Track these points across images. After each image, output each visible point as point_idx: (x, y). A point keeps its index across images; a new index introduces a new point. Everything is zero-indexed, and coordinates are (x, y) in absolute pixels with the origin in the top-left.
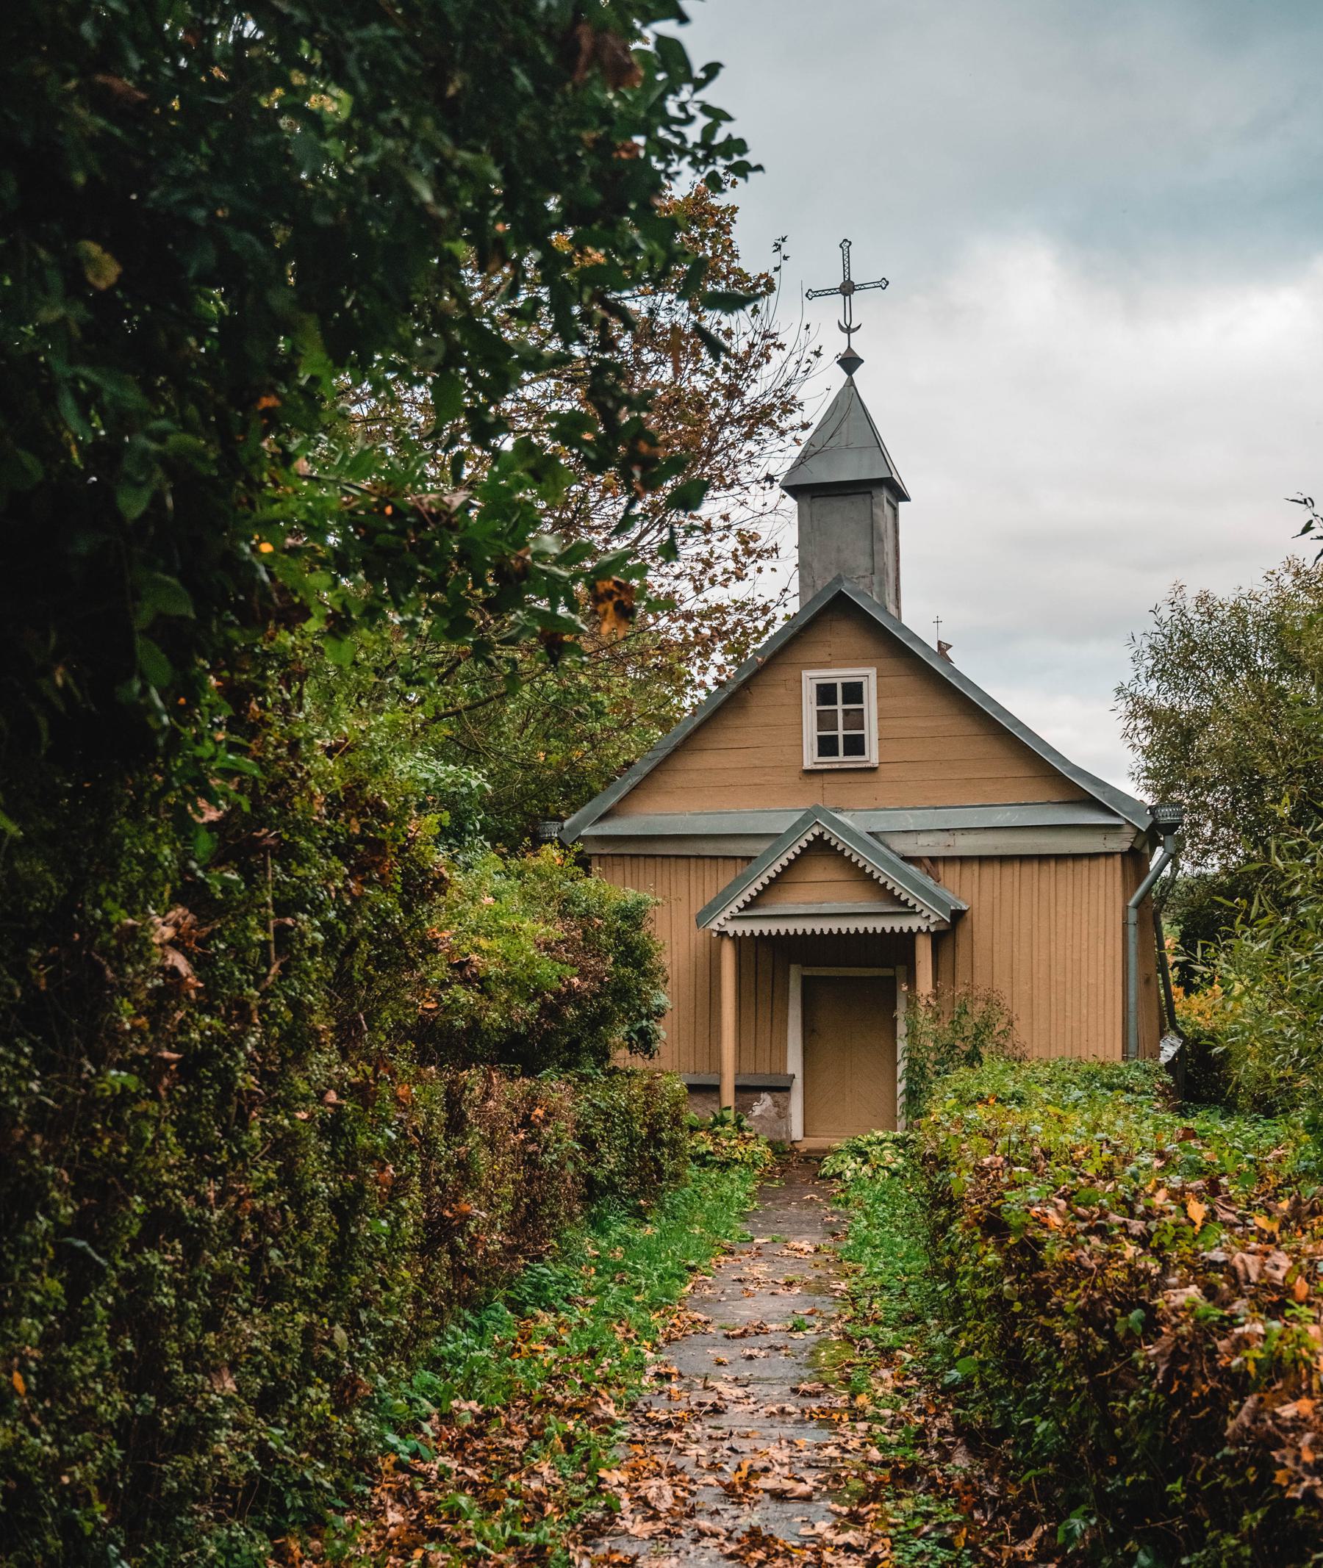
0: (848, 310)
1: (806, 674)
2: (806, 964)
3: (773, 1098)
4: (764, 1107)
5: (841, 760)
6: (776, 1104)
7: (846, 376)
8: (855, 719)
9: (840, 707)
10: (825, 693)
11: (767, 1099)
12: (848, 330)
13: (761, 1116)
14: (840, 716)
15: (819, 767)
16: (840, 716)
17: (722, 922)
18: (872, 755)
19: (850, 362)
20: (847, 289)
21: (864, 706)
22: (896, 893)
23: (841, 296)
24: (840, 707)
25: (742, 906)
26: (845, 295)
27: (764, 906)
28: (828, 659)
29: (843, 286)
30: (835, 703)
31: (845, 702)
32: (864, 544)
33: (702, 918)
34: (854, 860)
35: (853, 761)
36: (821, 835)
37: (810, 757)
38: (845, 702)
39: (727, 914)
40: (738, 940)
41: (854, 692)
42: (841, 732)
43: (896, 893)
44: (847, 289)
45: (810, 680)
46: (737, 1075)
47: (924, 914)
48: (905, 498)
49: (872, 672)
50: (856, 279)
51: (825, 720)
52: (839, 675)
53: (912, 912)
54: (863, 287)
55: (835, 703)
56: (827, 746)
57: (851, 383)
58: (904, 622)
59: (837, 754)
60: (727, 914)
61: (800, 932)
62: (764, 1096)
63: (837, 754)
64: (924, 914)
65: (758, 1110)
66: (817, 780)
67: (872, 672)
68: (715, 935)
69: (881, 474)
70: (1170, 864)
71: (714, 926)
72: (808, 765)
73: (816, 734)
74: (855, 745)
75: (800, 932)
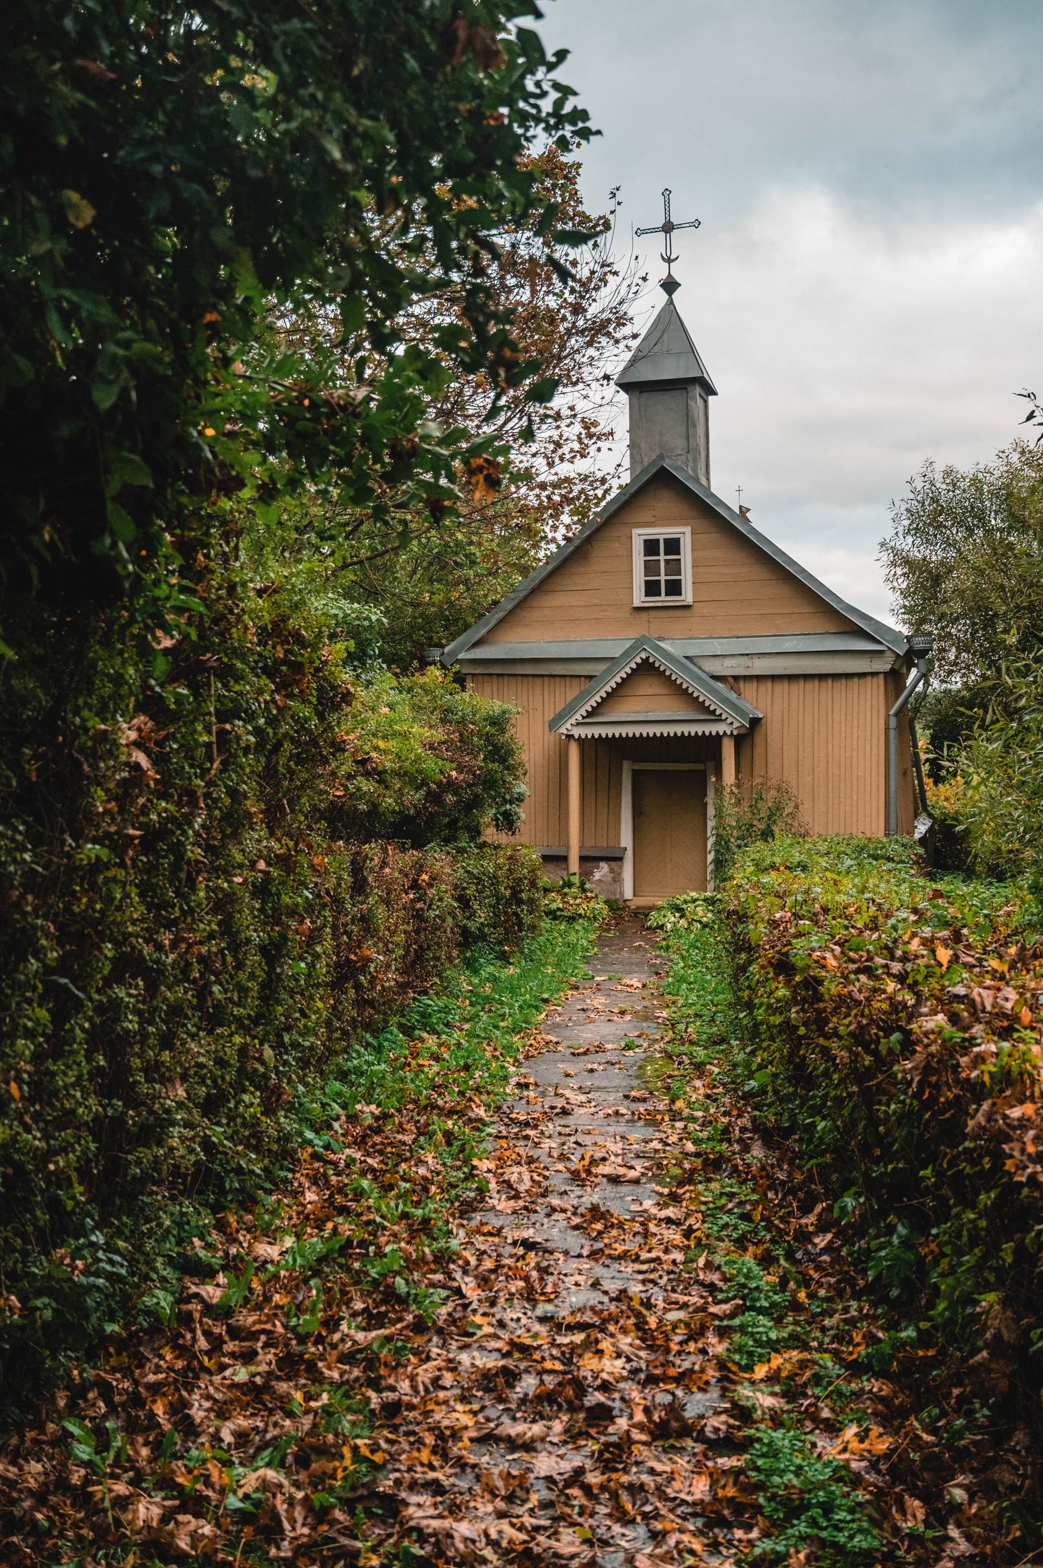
0: (668, 244)
1: (636, 532)
2: (635, 760)
5: (663, 599)
6: (612, 871)
7: (667, 297)
8: (674, 567)
9: (662, 557)
10: (651, 547)
12: (669, 261)
14: (662, 564)
16: (662, 564)
18: (688, 596)
19: (670, 286)
20: (668, 228)
21: (681, 557)
23: (663, 234)
27: (602, 714)
29: (664, 225)
31: (666, 554)
33: (554, 724)
36: (648, 658)
37: (639, 598)
38: (666, 554)
39: (573, 721)
40: (582, 742)
41: (673, 546)
42: (663, 578)
44: (668, 228)
45: (639, 536)
46: (581, 848)
48: (714, 393)
49: (688, 530)
50: (675, 220)
51: (650, 568)
52: (661, 533)
53: (719, 720)
54: (680, 226)
56: (652, 588)
57: (671, 302)
60: (573, 721)
62: (602, 864)
65: (597, 875)
67: (688, 530)
71: (563, 730)
72: (637, 603)
73: (644, 579)
74: (674, 588)
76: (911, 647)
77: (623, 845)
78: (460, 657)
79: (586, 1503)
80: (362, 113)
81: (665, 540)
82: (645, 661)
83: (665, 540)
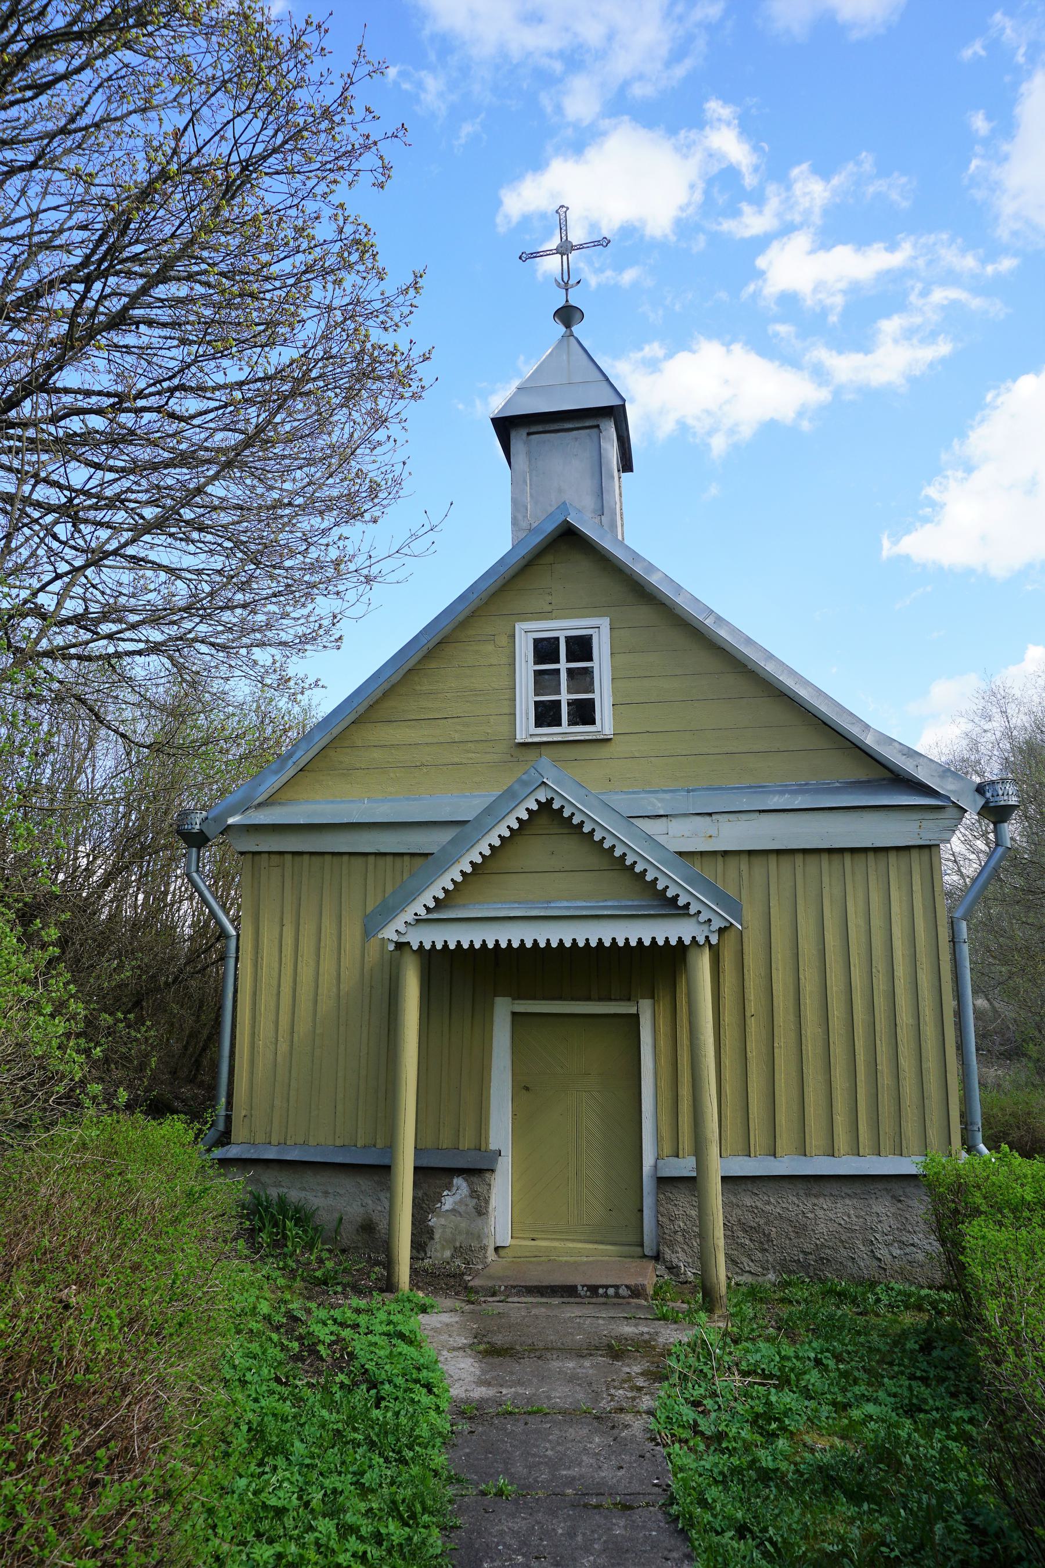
1: (520, 627)
2: (518, 996)
3: (470, 1185)
4: (457, 1197)
5: (565, 730)
6: (474, 1194)
8: (582, 678)
9: (563, 665)
10: (545, 650)
11: (460, 1183)
13: (453, 1211)
14: (564, 676)
15: (530, 740)
16: (564, 676)
17: (402, 928)
18: (605, 722)
21: (595, 664)
22: (660, 886)
24: (563, 665)
25: (432, 904)
26: (562, 254)
27: (464, 906)
28: (549, 608)
30: (558, 662)
31: (568, 660)
32: (588, 484)
33: (370, 927)
34: (597, 837)
35: (582, 731)
37: (526, 728)
38: (568, 660)
39: (408, 916)
41: (581, 647)
42: (565, 697)
43: (660, 886)
46: (417, 1150)
47: (703, 918)
49: (605, 623)
51: (544, 680)
55: (558, 662)
56: (547, 715)
58: (626, 542)
59: (559, 724)
60: (408, 916)
61: (516, 944)
62: (458, 1181)
63: (559, 724)
64: (703, 918)
65: (449, 1202)
66: (531, 754)
67: (605, 623)
68: (391, 947)
69: (606, 400)
70: (53, 244)
71: (389, 933)
72: (521, 737)
73: (533, 699)
74: (584, 713)
75: (516, 944)
76: (546, 79)
77: (493, 1146)
78: (231, 821)
79: (718, 228)
80: (954, 304)
81: (568, 639)
82: (545, 806)
83: (568, 639)
